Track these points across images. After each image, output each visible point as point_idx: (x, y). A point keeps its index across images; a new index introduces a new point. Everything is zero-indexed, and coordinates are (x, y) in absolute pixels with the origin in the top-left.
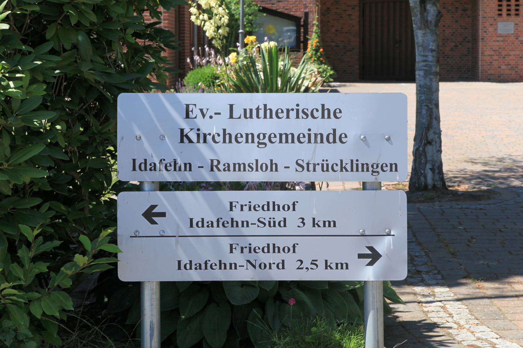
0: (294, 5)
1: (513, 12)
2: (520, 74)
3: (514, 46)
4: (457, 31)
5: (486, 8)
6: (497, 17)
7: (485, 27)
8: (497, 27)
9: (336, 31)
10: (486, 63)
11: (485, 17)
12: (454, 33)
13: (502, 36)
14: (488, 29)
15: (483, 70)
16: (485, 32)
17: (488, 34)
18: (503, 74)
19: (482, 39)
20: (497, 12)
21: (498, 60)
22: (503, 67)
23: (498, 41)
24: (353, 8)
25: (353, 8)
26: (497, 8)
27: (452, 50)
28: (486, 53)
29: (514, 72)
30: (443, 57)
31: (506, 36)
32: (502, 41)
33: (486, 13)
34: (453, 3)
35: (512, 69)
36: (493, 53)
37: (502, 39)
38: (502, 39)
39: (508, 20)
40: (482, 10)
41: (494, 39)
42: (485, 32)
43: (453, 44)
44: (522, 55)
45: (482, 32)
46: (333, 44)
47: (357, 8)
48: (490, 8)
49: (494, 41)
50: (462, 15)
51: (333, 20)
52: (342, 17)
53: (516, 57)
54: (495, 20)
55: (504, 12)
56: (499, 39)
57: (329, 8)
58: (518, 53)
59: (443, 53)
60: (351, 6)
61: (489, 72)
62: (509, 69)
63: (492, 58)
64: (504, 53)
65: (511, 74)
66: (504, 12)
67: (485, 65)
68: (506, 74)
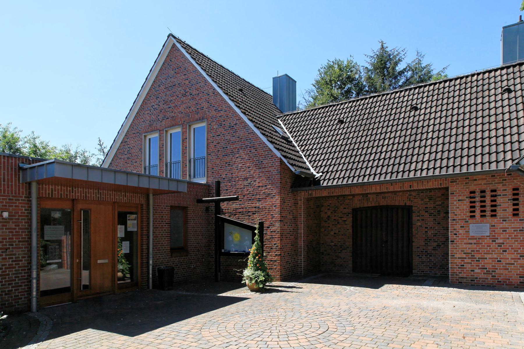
0: (264, 216)
1: (488, 213)
2: (498, 279)
3: (490, 249)
4: (440, 232)
5: (456, 210)
6: (469, 219)
7: (454, 229)
8: (469, 229)
9: (335, 233)
10: (456, 265)
11: (454, 220)
12: (436, 234)
13: (476, 239)
14: (459, 232)
15: (454, 273)
16: (456, 234)
17: (459, 237)
18: (477, 278)
19: (451, 241)
20: (469, 214)
21: (471, 263)
22: (477, 271)
23: (472, 244)
24: (347, 215)
25: (347, 215)
26: (468, 209)
27: (434, 249)
28: (457, 256)
29: (490, 277)
30: (425, 255)
31: (479, 239)
32: (474, 244)
33: (456, 215)
34: (435, 207)
35: (488, 273)
36: (464, 256)
37: (475, 241)
38: (475, 241)
39: (482, 222)
40: (451, 213)
41: (465, 241)
42: (456, 234)
43: (436, 244)
44: (2, 255)
45: (451, 234)
46: (333, 244)
47: (351, 215)
48: (460, 210)
49: (465, 244)
50: (444, 217)
51: (333, 225)
52: (339, 223)
53: (492, 261)
54: (468, 222)
55: (478, 214)
56: (470, 241)
57: (329, 216)
58: (495, 256)
59: (426, 252)
60: (346, 214)
61: (460, 275)
62: (484, 273)
63: (464, 261)
64: (477, 256)
65: (487, 279)
66: (478, 214)
67: (456, 268)
68: (480, 278)
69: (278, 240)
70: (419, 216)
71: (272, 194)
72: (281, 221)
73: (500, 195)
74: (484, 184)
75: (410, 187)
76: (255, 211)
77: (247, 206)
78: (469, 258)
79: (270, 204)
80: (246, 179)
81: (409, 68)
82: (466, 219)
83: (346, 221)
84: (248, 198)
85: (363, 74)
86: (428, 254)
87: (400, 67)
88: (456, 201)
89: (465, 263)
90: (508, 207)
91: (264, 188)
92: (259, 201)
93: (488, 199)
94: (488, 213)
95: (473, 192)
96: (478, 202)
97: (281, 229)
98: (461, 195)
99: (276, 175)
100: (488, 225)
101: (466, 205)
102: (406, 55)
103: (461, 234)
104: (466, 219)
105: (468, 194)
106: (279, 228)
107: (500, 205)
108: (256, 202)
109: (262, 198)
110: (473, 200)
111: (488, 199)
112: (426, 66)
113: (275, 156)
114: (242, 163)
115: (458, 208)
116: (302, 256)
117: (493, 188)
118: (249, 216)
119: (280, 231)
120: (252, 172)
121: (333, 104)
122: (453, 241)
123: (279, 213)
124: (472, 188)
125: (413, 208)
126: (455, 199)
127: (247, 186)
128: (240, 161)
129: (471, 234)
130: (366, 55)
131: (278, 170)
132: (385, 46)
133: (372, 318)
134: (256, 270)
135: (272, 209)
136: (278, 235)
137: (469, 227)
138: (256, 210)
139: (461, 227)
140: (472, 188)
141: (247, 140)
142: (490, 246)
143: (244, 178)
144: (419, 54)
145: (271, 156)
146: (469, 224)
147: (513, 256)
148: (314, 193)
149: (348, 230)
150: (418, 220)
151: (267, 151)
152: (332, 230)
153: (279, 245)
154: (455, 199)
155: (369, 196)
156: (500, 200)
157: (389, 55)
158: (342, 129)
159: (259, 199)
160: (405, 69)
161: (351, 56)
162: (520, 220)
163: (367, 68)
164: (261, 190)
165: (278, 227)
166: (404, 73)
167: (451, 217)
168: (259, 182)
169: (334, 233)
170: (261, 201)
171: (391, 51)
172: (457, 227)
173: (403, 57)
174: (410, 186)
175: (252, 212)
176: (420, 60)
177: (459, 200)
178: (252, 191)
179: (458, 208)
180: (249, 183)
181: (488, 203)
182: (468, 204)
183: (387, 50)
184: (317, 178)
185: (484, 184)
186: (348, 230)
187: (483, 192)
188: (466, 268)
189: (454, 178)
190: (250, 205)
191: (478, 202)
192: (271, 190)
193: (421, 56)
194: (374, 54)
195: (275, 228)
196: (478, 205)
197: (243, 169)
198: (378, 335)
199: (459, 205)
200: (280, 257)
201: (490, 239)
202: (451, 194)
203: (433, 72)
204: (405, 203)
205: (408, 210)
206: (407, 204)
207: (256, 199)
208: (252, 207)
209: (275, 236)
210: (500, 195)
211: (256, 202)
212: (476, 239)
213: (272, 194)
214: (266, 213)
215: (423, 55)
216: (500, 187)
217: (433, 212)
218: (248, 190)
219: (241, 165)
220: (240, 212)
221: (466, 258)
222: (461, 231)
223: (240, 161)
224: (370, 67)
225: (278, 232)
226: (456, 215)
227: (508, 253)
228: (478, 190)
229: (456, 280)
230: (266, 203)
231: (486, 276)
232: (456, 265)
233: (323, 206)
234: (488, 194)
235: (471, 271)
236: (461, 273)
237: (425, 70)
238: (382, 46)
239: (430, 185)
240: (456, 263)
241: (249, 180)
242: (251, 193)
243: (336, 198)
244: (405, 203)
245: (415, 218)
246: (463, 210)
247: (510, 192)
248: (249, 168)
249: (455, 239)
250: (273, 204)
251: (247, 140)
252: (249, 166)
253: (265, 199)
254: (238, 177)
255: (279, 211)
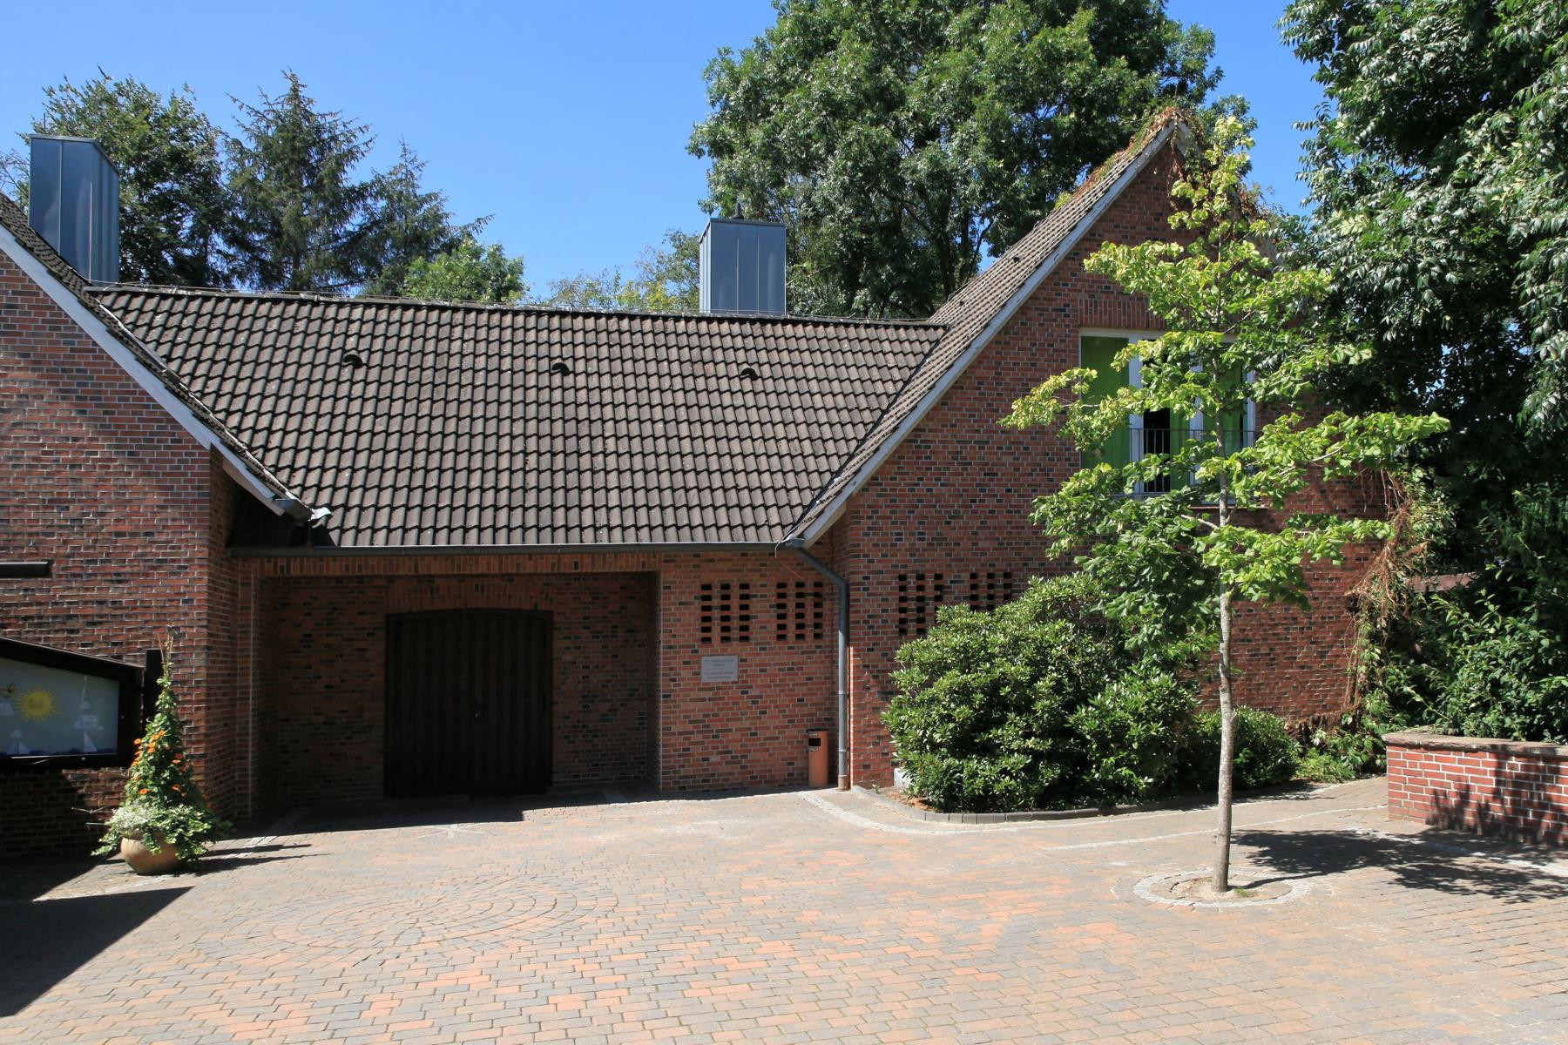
1: (735, 634)
7: (671, 669)
10: (675, 750)
11: (670, 647)
15: (671, 767)
16: (674, 680)
18: (713, 775)
20: (700, 635)
21: (703, 743)
23: (704, 700)
25: (369, 634)
26: (699, 624)
28: (674, 729)
31: (718, 688)
32: (710, 699)
33: (674, 636)
36: (690, 727)
37: (710, 695)
38: (710, 695)
39: (724, 652)
40: (665, 631)
42: (674, 680)
48: (683, 625)
52: (341, 656)
54: (697, 651)
55: (716, 634)
56: (703, 695)
58: (747, 724)
59: (584, 727)
61: (682, 772)
62: (728, 763)
66: (716, 634)
69: (198, 709)
70: (569, 638)
71: (174, 561)
72: (208, 648)
73: (756, 596)
74: (729, 571)
75: (576, 567)
76: (101, 616)
77: (62, 597)
78: (699, 732)
79: (166, 595)
80: (58, 502)
81: (379, 188)
82: (693, 646)
83: (364, 650)
84: (66, 568)
85: (222, 158)
86: (589, 731)
87: (354, 176)
88: (674, 604)
89: (690, 744)
90: (770, 622)
91: (140, 540)
92: (120, 582)
93: (735, 603)
94: (735, 634)
95: (706, 587)
96: (716, 608)
97: (208, 675)
98: (683, 593)
99: (194, 501)
100: (735, 658)
101: (693, 614)
102: (370, 145)
103: (683, 680)
104: (693, 646)
105: (700, 593)
106: (203, 671)
107: (756, 617)
108: (103, 585)
109: (132, 574)
110: (707, 603)
111: (735, 603)
112: (429, 196)
113: (188, 441)
114: (43, 445)
115: (679, 620)
116: (246, 758)
117: (745, 580)
118: (72, 631)
119: (207, 682)
120: (87, 483)
121: (311, 297)
122: (669, 696)
123: (204, 623)
124: (706, 579)
125: (556, 618)
126: (673, 599)
127: (61, 527)
128: (32, 438)
129: (705, 678)
130: (235, 100)
131: (199, 488)
132: (303, 93)
133: (297, 972)
134: (167, 806)
135: (173, 610)
136: (200, 693)
137: (699, 663)
138: (106, 611)
139: (685, 663)
140: (707, 578)
141: (64, 370)
142: (737, 703)
143: (51, 501)
144: (410, 157)
145: (173, 441)
146: (700, 657)
147: (777, 722)
148: (295, 564)
149: (372, 675)
150: (567, 648)
151: (160, 421)
152: (320, 677)
153: (202, 724)
154: (673, 599)
155: (437, 581)
156: (756, 606)
157: (318, 130)
158: (360, 384)
159: (118, 574)
160: (364, 187)
161: (186, 89)
162: (789, 648)
163: (237, 142)
164: (130, 547)
165: (199, 668)
166: (364, 198)
167: (665, 642)
168: (117, 521)
169: (327, 687)
170: (126, 581)
171: (323, 116)
172: (677, 663)
173: (363, 148)
174: (576, 564)
175: (85, 616)
176: (412, 175)
177: (680, 604)
178: (87, 548)
179: (679, 620)
180: (73, 520)
181: (735, 612)
182: (699, 614)
183: (314, 109)
184: (316, 521)
185: (729, 571)
186: (372, 675)
187: (726, 587)
188: (693, 755)
189: (671, 554)
190: (74, 593)
191: (716, 608)
192: (172, 548)
193: (416, 164)
194: (267, 108)
195: (189, 671)
196: (716, 614)
197: (44, 467)
198: (382, 997)
199: (681, 614)
200: (206, 762)
201: (738, 688)
202: (665, 588)
203: (449, 221)
204: (536, 605)
205: (539, 625)
206: (541, 607)
207: (104, 575)
208: (86, 603)
209: (184, 695)
210: (756, 596)
211: (103, 585)
212: (712, 689)
213: (174, 561)
214: (146, 622)
215: (419, 162)
216: (755, 579)
217: (600, 628)
218: (65, 542)
219: (34, 454)
220: (27, 618)
221: (692, 733)
222: (684, 674)
223: (32, 438)
224: (250, 145)
225: (197, 682)
226: (674, 636)
227: (770, 717)
228: (716, 584)
229: (675, 783)
230: (148, 590)
231: (728, 769)
232: (675, 750)
233: (288, 604)
234: (735, 592)
235: (704, 760)
236: (683, 766)
237: (426, 206)
238: (295, 90)
239: (622, 566)
240: (673, 745)
241: (74, 510)
242: (80, 555)
243: (333, 583)
244: (536, 605)
245: (559, 643)
246: (690, 624)
247: (773, 591)
248: (72, 467)
249: (671, 691)
250: (179, 594)
251: (64, 370)
252: (75, 460)
253: (147, 575)
254: (17, 494)
255: (205, 616)
